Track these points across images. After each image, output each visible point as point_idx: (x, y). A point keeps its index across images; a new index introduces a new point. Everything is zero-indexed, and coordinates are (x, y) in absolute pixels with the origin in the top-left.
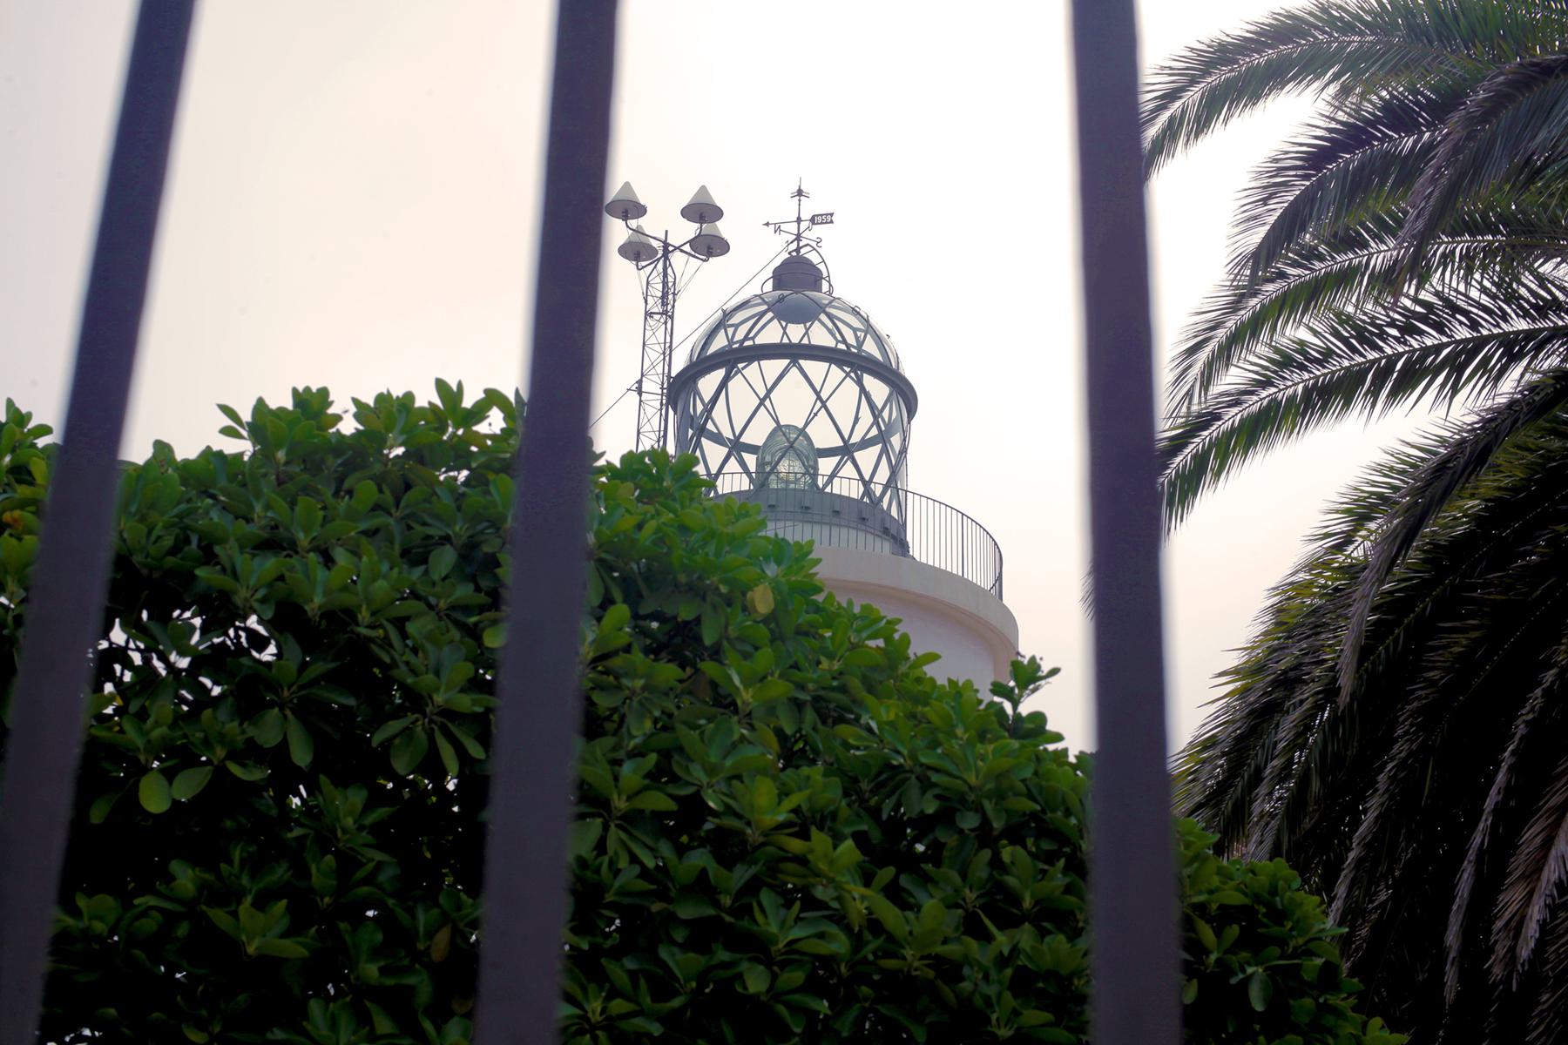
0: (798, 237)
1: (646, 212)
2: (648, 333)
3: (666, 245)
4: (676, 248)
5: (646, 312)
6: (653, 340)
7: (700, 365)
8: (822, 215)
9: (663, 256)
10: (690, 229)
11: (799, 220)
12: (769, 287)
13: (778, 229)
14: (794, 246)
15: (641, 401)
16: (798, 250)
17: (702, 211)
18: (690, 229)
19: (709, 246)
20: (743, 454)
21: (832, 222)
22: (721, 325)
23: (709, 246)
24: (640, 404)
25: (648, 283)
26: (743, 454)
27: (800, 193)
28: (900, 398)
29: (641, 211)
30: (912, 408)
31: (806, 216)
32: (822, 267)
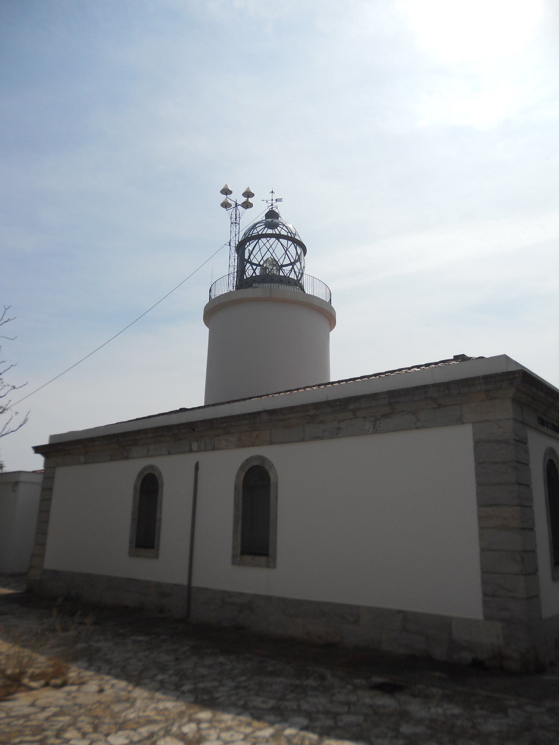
0: (272, 205)
1: (232, 193)
2: (232, 229)
3: (236, 204)
4: (239, 205)
5: (231, 222)
6: (233, 231)
7: (248, 238)
8: (279, 199)
9: (235, 206)
10: (244, 199)
11: (272, 200)
12: (264, 218)
13: (267, 202)
14: (271, 207)
15: (230, 248)
16: (272, 208)
17: (248, 194)
18: (244, 199)
19: (247, 205)
20: (253, 266)
21: (282, 201)
22: (254, 227)
23: (247, 205)
24: (230, 249)
25: (231, 214)
26: (253, 266)
27: (272, 192)
28: (302, 251)
29: (230, 192)
30: (305, 253)
31: (274, 199)
32: (278, 213)
